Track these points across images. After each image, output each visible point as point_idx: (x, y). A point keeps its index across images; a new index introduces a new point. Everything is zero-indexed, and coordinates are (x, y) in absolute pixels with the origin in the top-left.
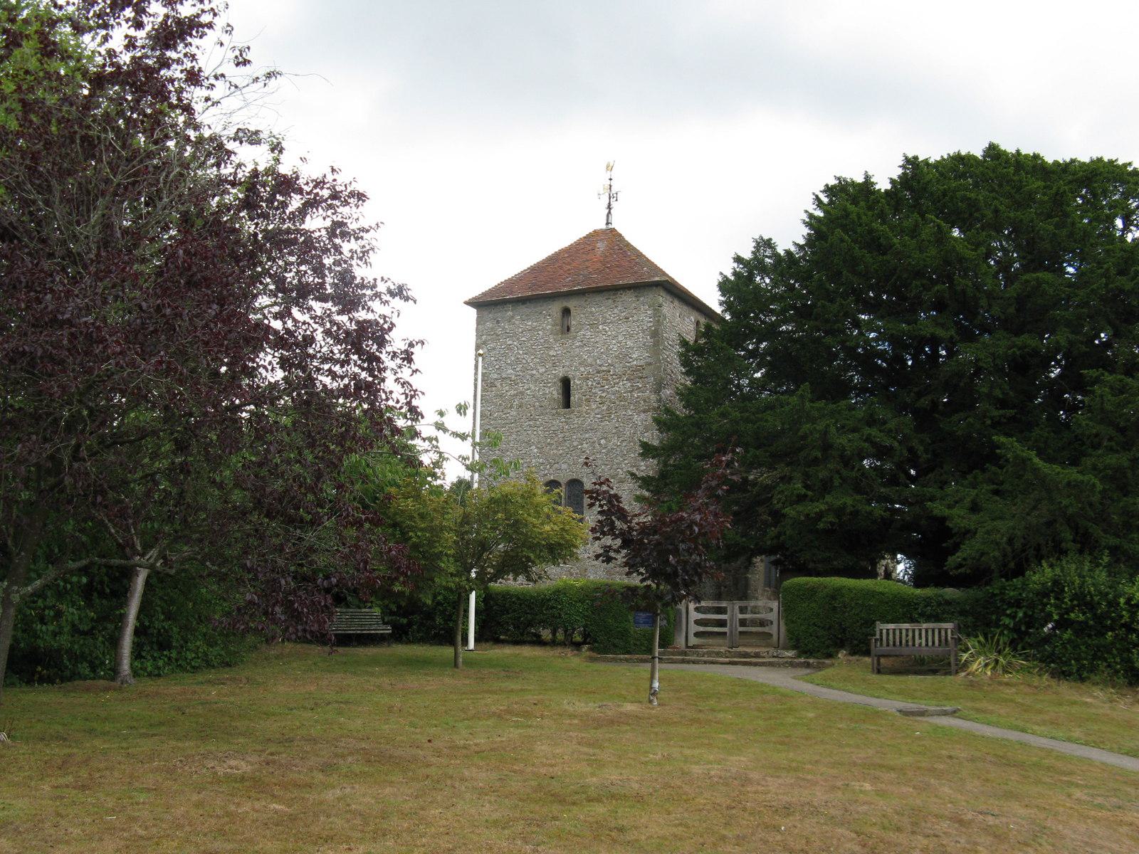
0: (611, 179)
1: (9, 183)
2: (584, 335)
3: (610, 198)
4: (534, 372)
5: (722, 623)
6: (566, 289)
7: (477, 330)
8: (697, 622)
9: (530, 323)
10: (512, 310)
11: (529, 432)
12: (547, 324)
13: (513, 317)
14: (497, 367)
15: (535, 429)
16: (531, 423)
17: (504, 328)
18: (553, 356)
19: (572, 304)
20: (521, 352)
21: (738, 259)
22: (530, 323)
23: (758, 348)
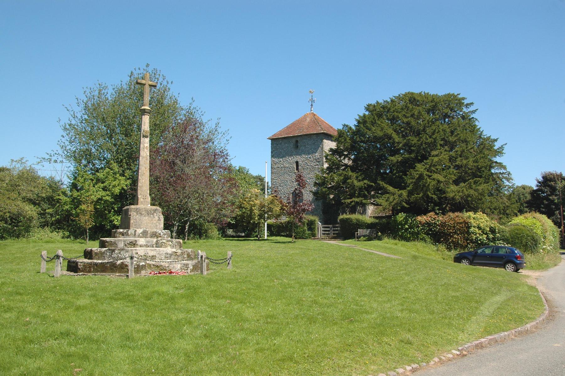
6: (296, 135)
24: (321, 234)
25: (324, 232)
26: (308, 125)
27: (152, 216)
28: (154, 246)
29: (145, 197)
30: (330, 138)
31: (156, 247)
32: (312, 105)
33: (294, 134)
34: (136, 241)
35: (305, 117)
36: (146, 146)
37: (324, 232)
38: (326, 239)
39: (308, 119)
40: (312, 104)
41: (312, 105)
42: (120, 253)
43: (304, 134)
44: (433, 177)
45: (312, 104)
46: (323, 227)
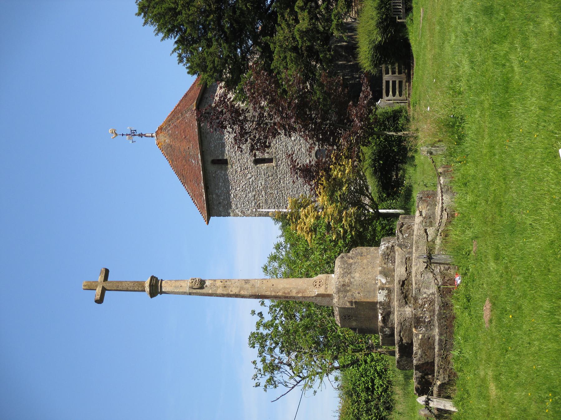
0: (123, 135)
1: (346, 250)
2: (228, 151)
3: (135, 135)
4: (251, 180)
5: (394, 83)
6: (200, 162)
7: (224, 216)
8: (394, 95)
9: (221, 184)
10: (212, 195)
11: (287, 182)
12: (221, 173)
13: (217, 194)
14: (247, 203)
15: (285, 179)
16: (282, 181)
17: (224, 199)
18: (241, 169)
19: (210, 159)
20: (238, 189)
21: (145, 23)
22: (221, 184)
23: (352, 235)
30: (207, 95)
32: (141, 135)
40: (139, 135)
41: (141, 135)
43: (198, 146)
45: (139, 135)
46: (387, 95)
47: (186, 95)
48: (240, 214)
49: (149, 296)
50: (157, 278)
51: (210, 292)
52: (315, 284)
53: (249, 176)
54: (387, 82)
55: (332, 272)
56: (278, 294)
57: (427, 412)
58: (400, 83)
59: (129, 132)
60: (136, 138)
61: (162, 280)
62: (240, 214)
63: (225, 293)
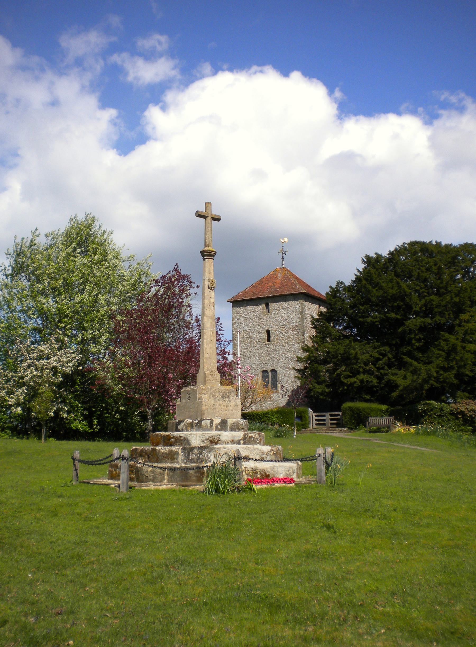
5: (324, 420)
6: (267, 296)
24: (314, 425)
25: (317, 422)
26: (281, 283)
27: (227, 399)
28: (242, 442)
29: (213, 373)
30: (310, 299)
31: (244, 444)
32: (283, 258)
33: (263, 295)
34: (219, 435)
35: (275, 272)
36: (212, 302)
37: (317, 422)
38: (321, 431)
39: (280, 276)
40: (283, 257)
41: (283, 258)
42: (201, 453)
43: (278, 294)
44: (467, 349)
45: (283, 257)
46: (316, 416)
47: (309, 286)
48: (234, 321)
49: (201, 250)
50: (214, 256)
51: (206, 294)
52: (213, 371)
53: (259, 327)
54: (324, 416)
55: (222, 383)
56: (205, 344)
57: (116, 456)
58: (324, 424)
59: (284, 250)
60: (281, 254)
61: (213, 259)
62: (234, 321)
63: (205, 305)
